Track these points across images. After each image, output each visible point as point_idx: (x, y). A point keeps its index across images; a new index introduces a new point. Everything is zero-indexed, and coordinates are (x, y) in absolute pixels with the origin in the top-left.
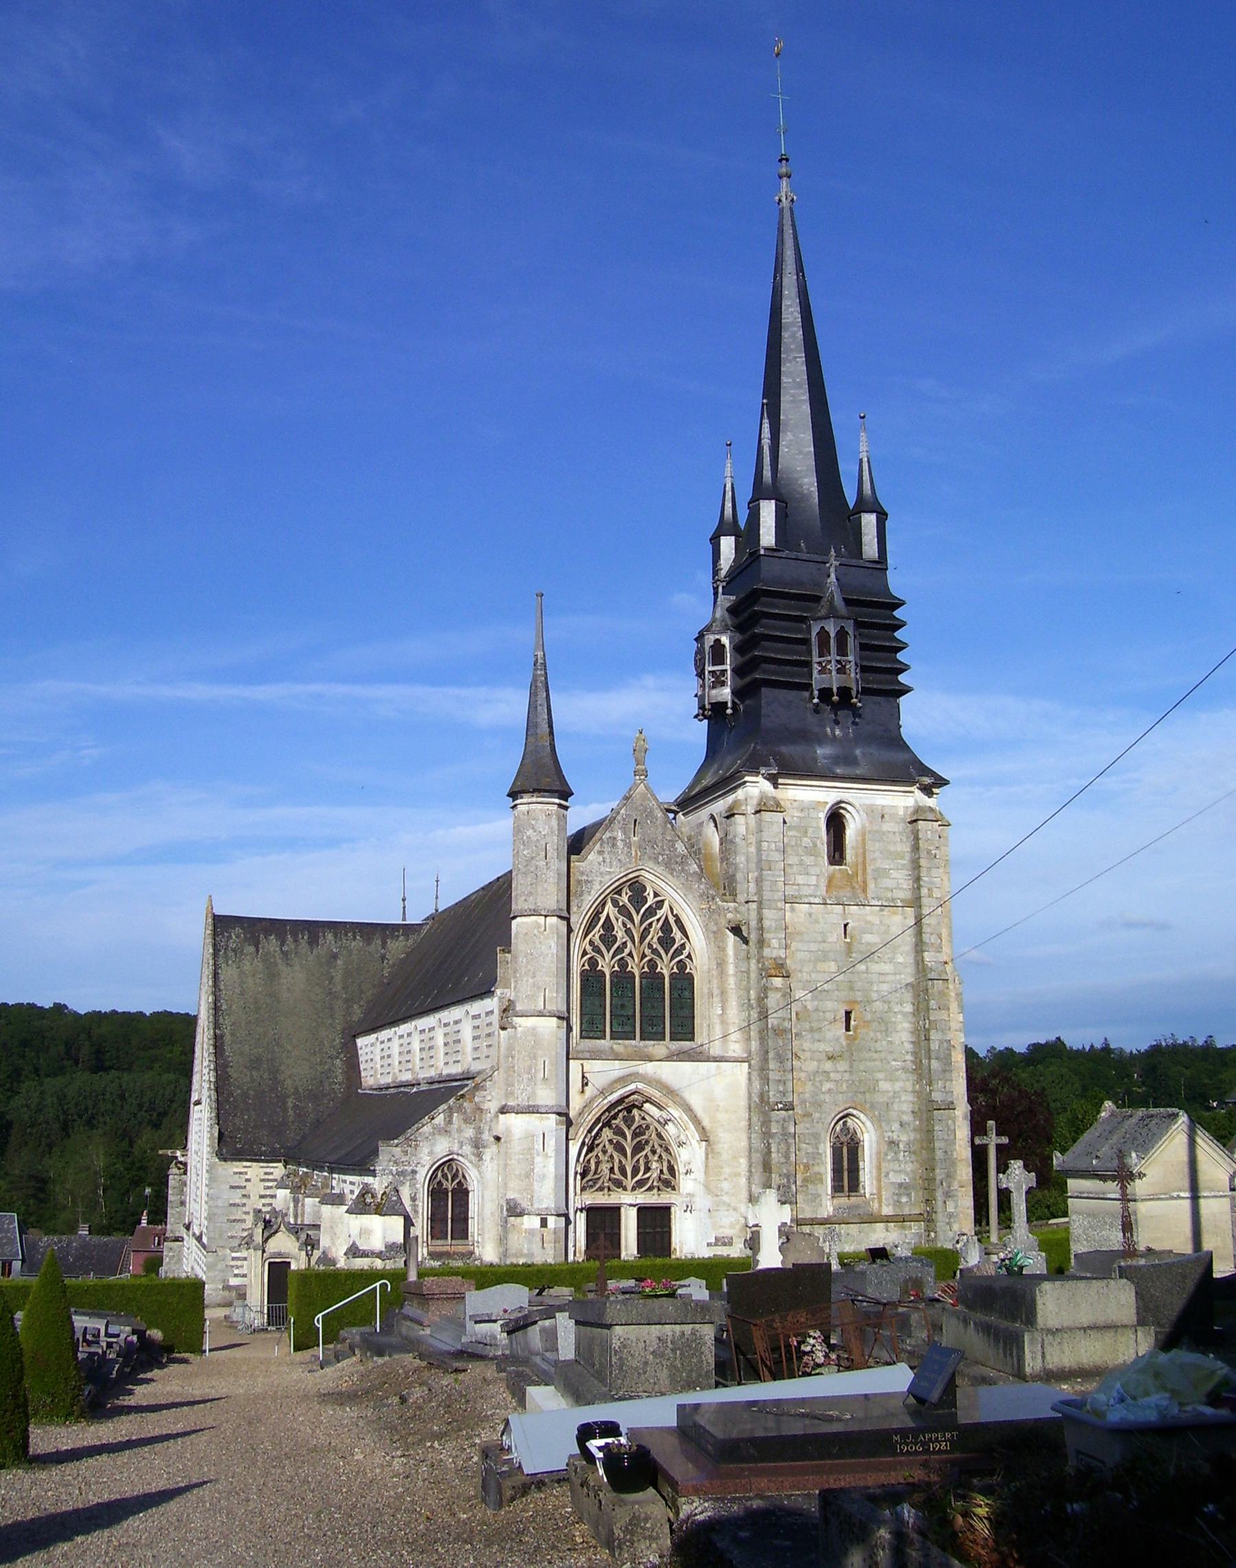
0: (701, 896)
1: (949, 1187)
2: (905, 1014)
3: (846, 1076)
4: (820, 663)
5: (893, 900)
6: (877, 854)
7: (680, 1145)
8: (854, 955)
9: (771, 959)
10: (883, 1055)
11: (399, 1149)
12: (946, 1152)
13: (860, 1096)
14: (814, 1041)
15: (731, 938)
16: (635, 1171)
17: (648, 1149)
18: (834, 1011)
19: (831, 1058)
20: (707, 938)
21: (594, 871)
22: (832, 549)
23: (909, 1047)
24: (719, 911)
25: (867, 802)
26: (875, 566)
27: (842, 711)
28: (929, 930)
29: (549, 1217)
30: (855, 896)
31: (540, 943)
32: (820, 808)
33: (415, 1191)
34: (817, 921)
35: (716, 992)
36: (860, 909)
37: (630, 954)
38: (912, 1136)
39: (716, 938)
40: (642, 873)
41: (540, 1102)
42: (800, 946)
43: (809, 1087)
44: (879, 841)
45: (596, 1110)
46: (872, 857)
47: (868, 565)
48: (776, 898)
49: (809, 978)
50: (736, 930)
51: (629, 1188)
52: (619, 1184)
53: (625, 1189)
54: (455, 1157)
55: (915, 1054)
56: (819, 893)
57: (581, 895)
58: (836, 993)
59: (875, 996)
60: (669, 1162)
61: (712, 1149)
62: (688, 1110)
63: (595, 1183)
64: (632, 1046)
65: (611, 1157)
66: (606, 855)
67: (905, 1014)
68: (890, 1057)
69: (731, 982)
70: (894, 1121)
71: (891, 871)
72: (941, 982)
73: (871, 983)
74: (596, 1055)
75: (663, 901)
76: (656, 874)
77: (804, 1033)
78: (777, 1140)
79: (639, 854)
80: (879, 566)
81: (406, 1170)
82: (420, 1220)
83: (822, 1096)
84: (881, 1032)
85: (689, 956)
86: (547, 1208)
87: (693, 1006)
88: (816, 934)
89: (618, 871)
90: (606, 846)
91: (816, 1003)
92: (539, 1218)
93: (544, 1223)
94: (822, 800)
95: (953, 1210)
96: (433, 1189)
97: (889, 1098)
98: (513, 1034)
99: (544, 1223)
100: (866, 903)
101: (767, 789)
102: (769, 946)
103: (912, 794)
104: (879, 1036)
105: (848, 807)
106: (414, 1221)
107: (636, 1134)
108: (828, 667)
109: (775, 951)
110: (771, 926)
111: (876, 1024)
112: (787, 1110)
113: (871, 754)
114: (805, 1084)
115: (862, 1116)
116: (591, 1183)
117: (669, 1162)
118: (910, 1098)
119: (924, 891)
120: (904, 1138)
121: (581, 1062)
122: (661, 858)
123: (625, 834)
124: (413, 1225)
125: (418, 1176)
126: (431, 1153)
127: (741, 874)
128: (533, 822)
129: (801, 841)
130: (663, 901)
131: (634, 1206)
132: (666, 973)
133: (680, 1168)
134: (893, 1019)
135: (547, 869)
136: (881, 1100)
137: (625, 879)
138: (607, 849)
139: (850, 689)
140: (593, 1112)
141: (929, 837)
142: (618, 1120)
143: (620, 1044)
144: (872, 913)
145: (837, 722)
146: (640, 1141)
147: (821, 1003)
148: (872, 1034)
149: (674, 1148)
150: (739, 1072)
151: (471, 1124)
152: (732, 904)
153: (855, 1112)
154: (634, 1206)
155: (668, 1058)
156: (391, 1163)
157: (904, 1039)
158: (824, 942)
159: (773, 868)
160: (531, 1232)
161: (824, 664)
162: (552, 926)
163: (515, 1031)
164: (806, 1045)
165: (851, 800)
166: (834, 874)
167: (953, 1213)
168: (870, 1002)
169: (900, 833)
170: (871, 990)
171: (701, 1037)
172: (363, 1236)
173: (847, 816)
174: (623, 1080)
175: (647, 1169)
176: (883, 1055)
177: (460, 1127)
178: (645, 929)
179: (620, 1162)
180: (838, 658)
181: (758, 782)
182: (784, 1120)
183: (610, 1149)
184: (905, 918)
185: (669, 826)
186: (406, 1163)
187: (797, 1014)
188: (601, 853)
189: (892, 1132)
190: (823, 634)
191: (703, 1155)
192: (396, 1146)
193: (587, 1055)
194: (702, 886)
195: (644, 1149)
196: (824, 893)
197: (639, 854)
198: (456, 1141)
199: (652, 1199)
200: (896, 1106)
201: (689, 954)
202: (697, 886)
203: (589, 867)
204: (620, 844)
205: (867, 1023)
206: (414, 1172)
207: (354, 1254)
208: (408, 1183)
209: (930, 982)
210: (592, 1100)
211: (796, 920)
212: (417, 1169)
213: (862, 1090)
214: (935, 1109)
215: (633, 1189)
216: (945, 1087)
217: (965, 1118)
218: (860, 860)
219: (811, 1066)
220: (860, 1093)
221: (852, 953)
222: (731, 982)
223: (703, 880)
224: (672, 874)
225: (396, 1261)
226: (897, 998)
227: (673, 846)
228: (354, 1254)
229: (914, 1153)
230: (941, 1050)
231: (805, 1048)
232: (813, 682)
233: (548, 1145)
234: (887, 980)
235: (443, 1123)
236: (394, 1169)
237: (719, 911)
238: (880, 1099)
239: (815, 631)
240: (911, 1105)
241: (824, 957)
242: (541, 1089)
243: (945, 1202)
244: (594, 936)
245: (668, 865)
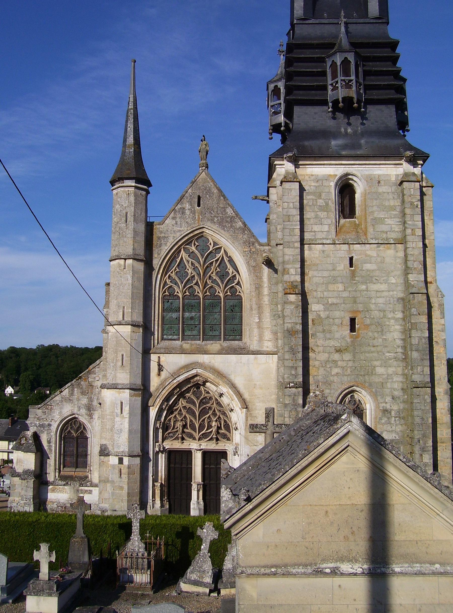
0: (244, 243)
1: (425, 444)
2: (396, 320)
3: (350, 364)
4: (332, 85)
5: (387, 239)
6: (375, 208)
7: (232, 410)
8: (357, 279)
9: (289, 282)
10: (379, 349)
11: (40, 411)
12: (422, 418)
13: (361, 378)
14: (326, 339)
15: (266, 270)
16: (201, 427)
17: (211, 412)
18: (342, 318)
19: (339, 351)
20: (249, 270)
21: (169, 230)
22: (343, 12)
23: (399, 342)
24: (257, 252)
25: (367, 173)
26: (377, 21)
27: (353, 117)
28: (412, 259)
29: (124, 457)
30: (358, 237)
31: (121, 277)
32: (331, 179)
33: (50, 437)
34: (328, 256)
35: (254, 306)
36: (361, 246)
37: (197, 284)
38: (402, 406)
39: (254, 270)
40: (204, 230)
41: (119, 381)
42: (315, 273)
43: (321, 371)
44: (376, 199)
45: (169, 386)
46: (370, 210)
47: (372, 21)
48: (293, 240)
49: (322, 296)
50: (269, 263)
51: (197, 438)
52: (191, 436)
53: (194, 439)
54: (77, 416)
55: (404, 348)
56: (330, 237)
57: (160, 247)
58: (343, 305)
59: (373, 307)
60: (225, 421)
61: (250, 414)
62: (233, 386)
63: (174, 435)
64: (196, 344)
65: (185, 417)
66: (178, 220)
67: (396, 320)
68: (385, 350)
69: (266, 300)
70: (387, 395)
71: (386, 220)
72: (420, 295)
73: (370, 298)
74: (169, 351)
75: (221, 248)
76: (213, 229)
77: (318, 334)
78: (289, 409)
79: (201, 217)
80: (380, 21)
81: (45, 424)
82: (53, 455)
83: (332, 378)
84: (378, 332)
85: (238, 283)
86: (123, 452)
87: (242, 318)
88: (327, 265)
89: (186, 229)
90: (178, 214)
91: (328, 313)
92: (117, 457)
93: (121, 461)
94: (332, 174)
95: (428, 461)
96: (65, 436)
97: (383, 379)
98: (106, 337)
99: (121, 461)
100: (366, 242)
101: (289, 168)
102: (288, 274)
103: (401, 166)
104: (376, 334)
105: (355, 178)
106: (49, 455)
107: (203, 403)
108: (337, 86)
109: (292, 277)
110: (290, 259)
111: (374, 326)
112: (297, 387)
113: (373, 142)
114: (319, 369)
115: (363, 392)
116: (171, 434)
117: (225, 421)
118: (400, 379)
119: (409, 231)
120: (395, 407)
121: (159, 355)
122: (216, 219)
123: (191, 205)
124: (49, 458)
125: (52, 428)
126: (60, 413)
127: (273, 227)
128: (119, 200)
129: (316, 202)
130: (221, 248)
131: (200, 450)
132: (221, 295)
133: (232, 427)
134: (388, 323)
135: (126, 229)
136: (377, 381)
137: (192, 235)
138: (178, 216)
139: (352, 98)
140: (167, 388)
141: (412, 193)
142: (191, 393)
143: (188, 343)
144: (371, 249)
145: (349, 124)
146: (205, 408)
147: (331, 312)
148: (370, 334)
149: (228, 412)
150: (271, 362)
151: (85, 395)
152: (267, 248)
153: (358, 389)
154: (200, 450)
155: (220, 353)
156: (36, 419)
157: (396, 337)
158: (334, 270)
159: (291, 219)
160: (113, 466)
161: (334, 85)
162: (129, 265)
163: (108, 335)
164: (320, 342)
165: (354, 172)
166: (345, 224)
167: (427, 463)
168: (368, 310)
169: (393, 193)
170: (370, 303)
171: (246, 338)
172: (18, 464)
173: (355, 185)
174: (188, 367)
175: (210, 427)
176: (379, 349)
177: (79, 397)
178: (207, 267)
179: (191, 421)
180: (343, 78)
181: (284, 165)
182: (295, 395)
183: (184, 412)
184: (397, 252)
185: (222, 198)
186: (45, 420)
187: (313, 321)
188: (174, 218)
189: (386, 403)
190: (334, 64)
191: (244, 417)
192: (39, 409)
193: (163, 351)
194: (245, 236)
195: (208, 413)
196: (334, 236)
197: (201, 217)
198: (76, 406)
199: (211, 446)
200: (389, 385)
201: (239, 282)
202: (241, 236)
203: (165, 228)
204: (188, 212)
205: (367, 326)
206: (50, 425)
207: (13, 475)
208: (46, 432)
209: (412, 296)
210: (165, 380)
211: (313, 256)
212: (52, 423)
213: (363, 373)
214: (414, 387)
215: (199, 440)
216: (423, 371)
217: (446, 393)
218: (363, 213)
219: (323, 357)
220: (361, 375)
221: (355, 277)
222: (266, 300)
223: (246, 232)
224: (223, 229)
225: (28, 481)
226: (390, 308)
227: (225, 211)
228: (13, 475)
229: (403, 418)
230: (421, 343)
231: (319, 344)
232: (328, 98)
233: (124, 410)
234: (382, 296)
235: (68, 394)
236: (38, 423)
237: (257, 252)
238: (376, 379)
239: (329, 63)
240: (401, 385)
241: (334, 280)
242: (120, 373)
243: (421, 455)
244: (172, 273)
245: (221, 224)
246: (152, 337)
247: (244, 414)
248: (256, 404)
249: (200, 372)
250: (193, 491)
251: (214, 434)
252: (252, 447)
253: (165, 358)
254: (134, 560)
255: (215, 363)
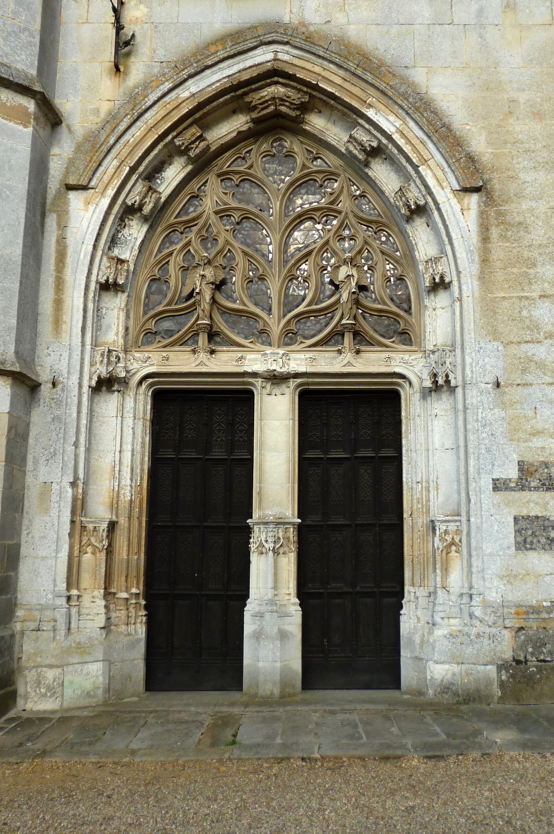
61: (499, 214)
246: (87, 446)
247: (473, 214)
248: (522, 176)
249: (286, 57)
250: (254, 558)
251: (347, 311)
252: (514, 350)
253: (145, 10)
254: (426, 585)
255: (349, 23)
